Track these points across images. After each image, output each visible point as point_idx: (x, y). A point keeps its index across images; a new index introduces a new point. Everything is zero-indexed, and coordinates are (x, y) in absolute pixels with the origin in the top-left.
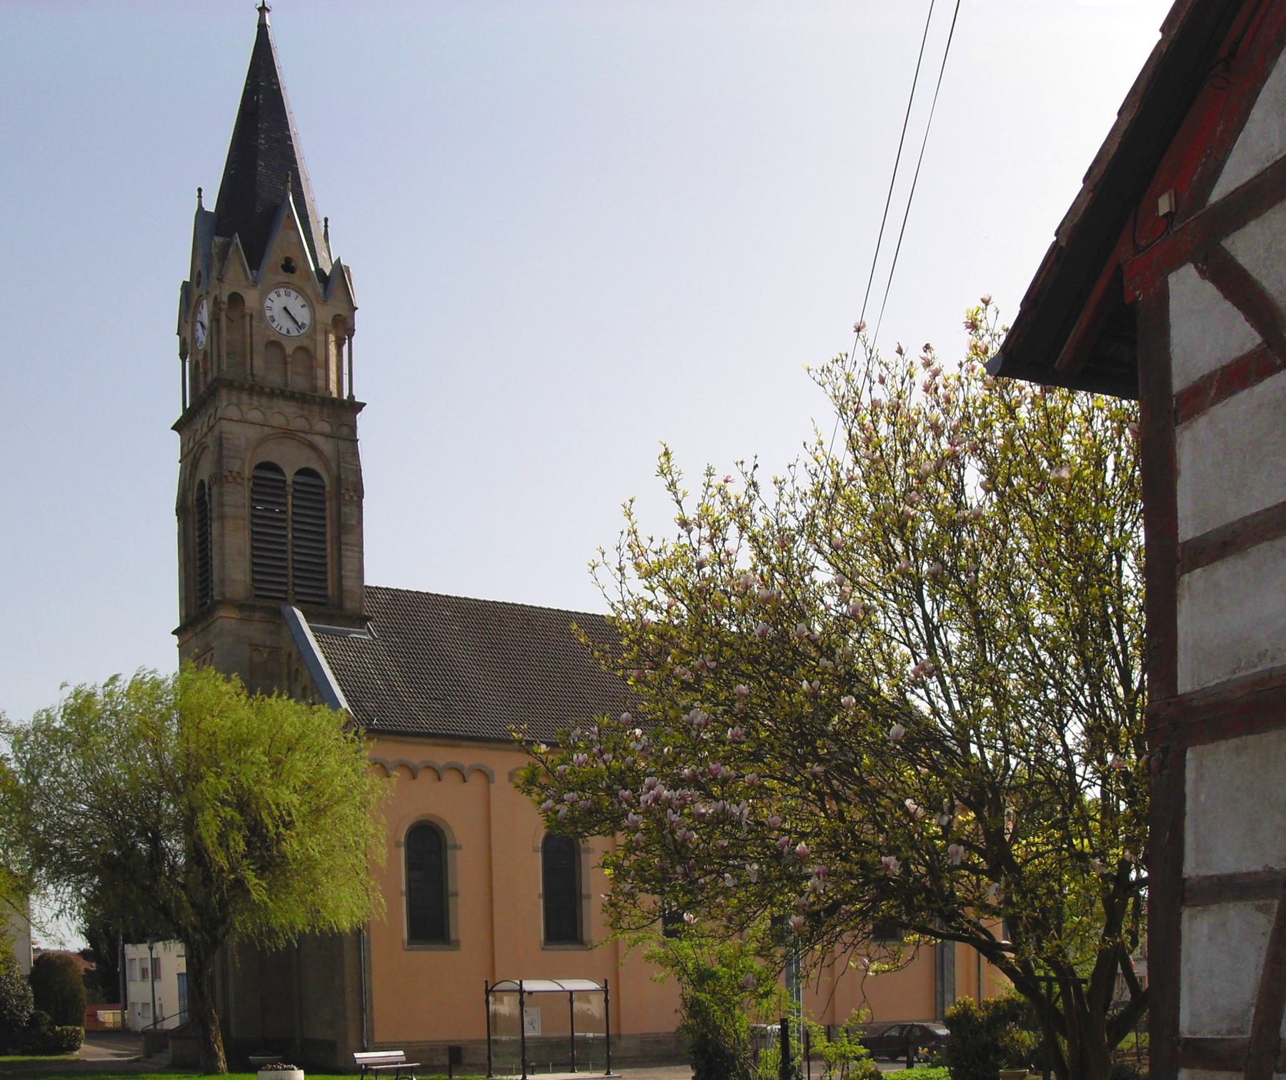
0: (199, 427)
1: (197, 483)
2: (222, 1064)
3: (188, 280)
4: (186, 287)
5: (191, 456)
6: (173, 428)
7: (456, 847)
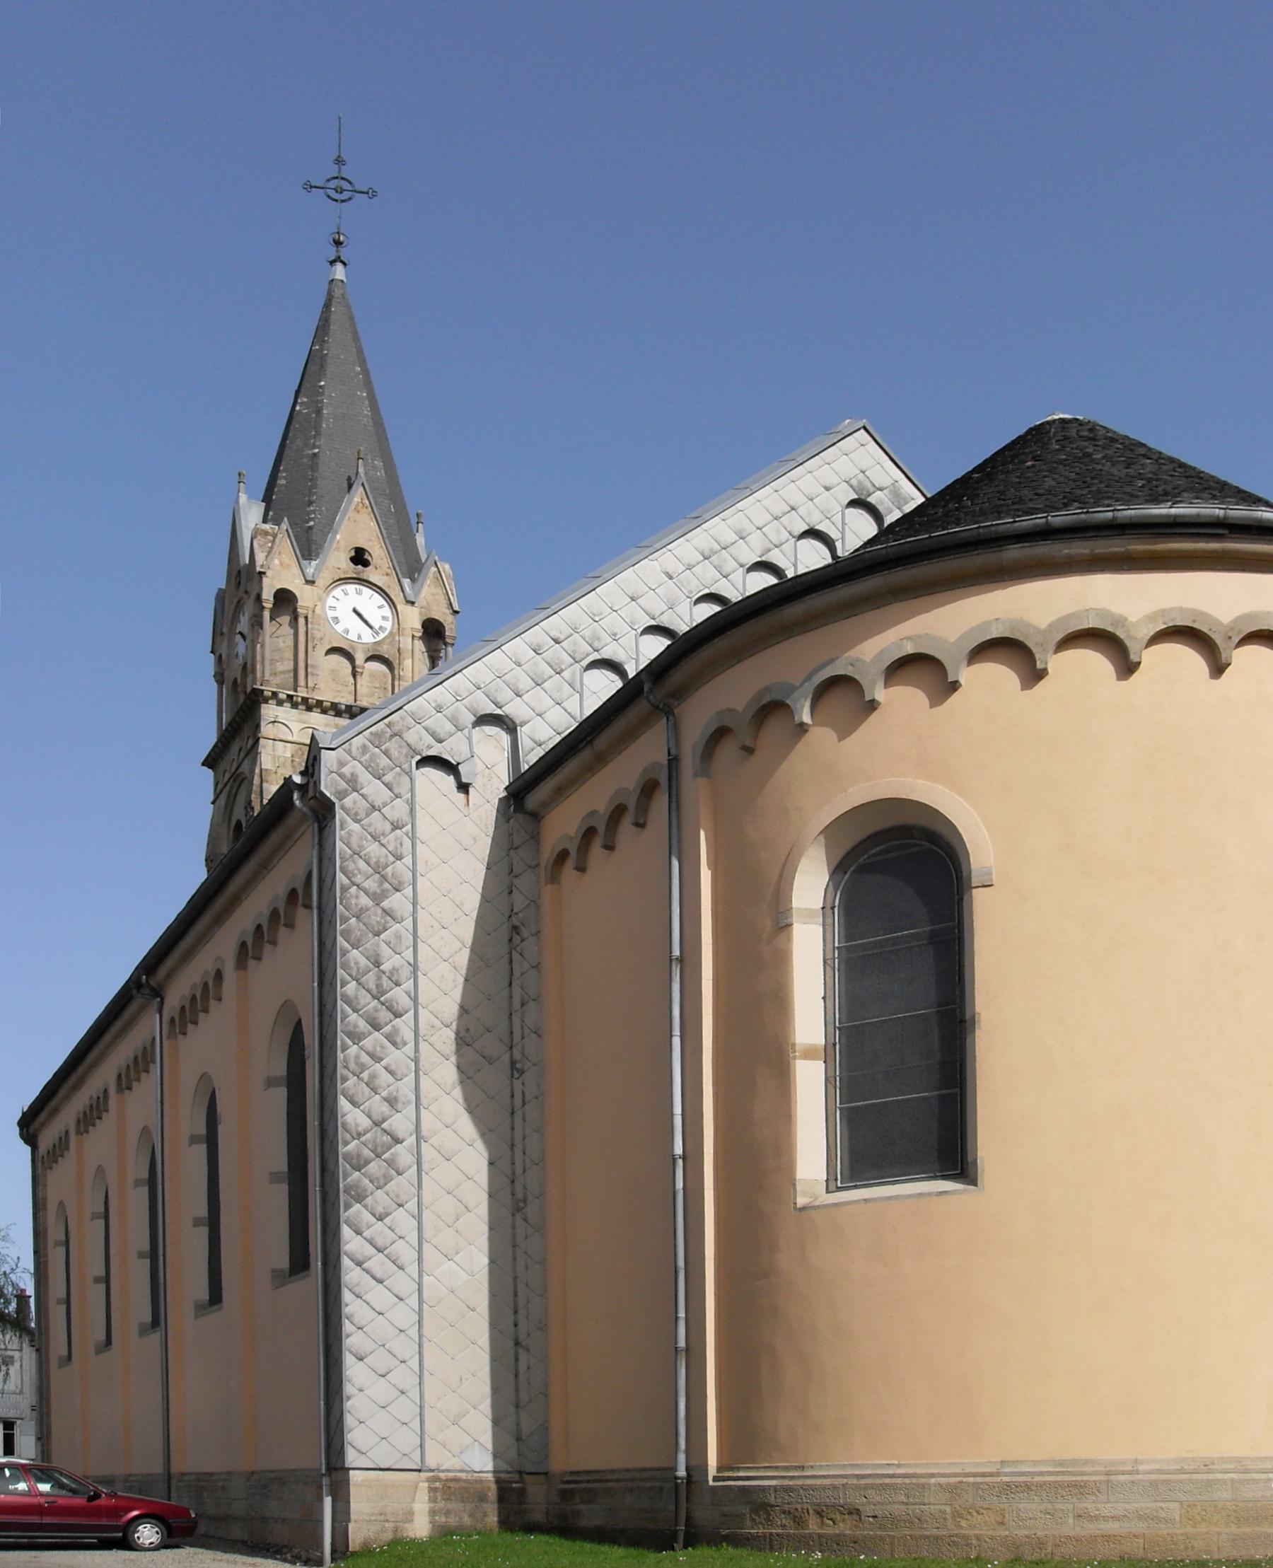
0: (236, 757)
1: (234, 823)
2: (6, 1432)
3: (224, 587)
4: (221, 597)
5: (223, 798)
6: (203, 764)
7: (979, 1014)
